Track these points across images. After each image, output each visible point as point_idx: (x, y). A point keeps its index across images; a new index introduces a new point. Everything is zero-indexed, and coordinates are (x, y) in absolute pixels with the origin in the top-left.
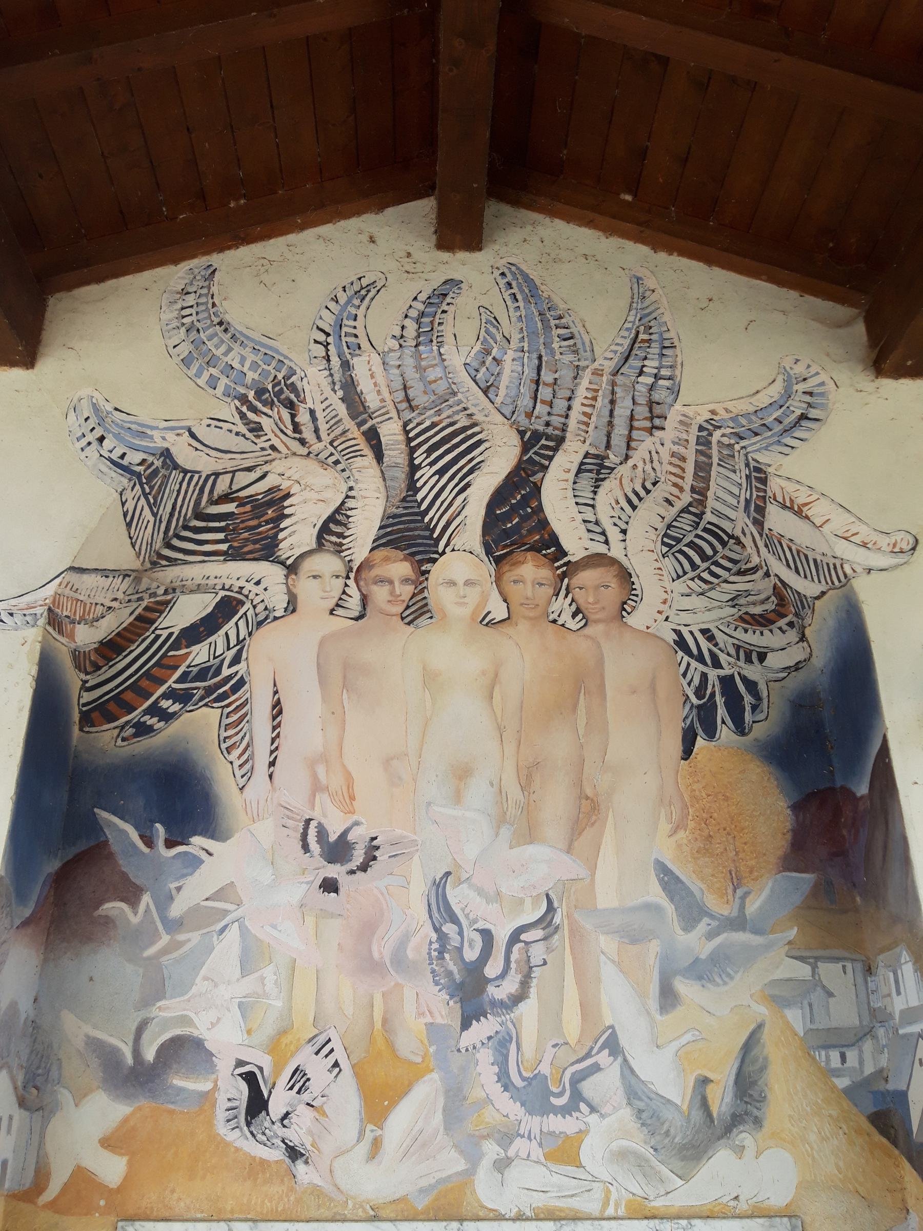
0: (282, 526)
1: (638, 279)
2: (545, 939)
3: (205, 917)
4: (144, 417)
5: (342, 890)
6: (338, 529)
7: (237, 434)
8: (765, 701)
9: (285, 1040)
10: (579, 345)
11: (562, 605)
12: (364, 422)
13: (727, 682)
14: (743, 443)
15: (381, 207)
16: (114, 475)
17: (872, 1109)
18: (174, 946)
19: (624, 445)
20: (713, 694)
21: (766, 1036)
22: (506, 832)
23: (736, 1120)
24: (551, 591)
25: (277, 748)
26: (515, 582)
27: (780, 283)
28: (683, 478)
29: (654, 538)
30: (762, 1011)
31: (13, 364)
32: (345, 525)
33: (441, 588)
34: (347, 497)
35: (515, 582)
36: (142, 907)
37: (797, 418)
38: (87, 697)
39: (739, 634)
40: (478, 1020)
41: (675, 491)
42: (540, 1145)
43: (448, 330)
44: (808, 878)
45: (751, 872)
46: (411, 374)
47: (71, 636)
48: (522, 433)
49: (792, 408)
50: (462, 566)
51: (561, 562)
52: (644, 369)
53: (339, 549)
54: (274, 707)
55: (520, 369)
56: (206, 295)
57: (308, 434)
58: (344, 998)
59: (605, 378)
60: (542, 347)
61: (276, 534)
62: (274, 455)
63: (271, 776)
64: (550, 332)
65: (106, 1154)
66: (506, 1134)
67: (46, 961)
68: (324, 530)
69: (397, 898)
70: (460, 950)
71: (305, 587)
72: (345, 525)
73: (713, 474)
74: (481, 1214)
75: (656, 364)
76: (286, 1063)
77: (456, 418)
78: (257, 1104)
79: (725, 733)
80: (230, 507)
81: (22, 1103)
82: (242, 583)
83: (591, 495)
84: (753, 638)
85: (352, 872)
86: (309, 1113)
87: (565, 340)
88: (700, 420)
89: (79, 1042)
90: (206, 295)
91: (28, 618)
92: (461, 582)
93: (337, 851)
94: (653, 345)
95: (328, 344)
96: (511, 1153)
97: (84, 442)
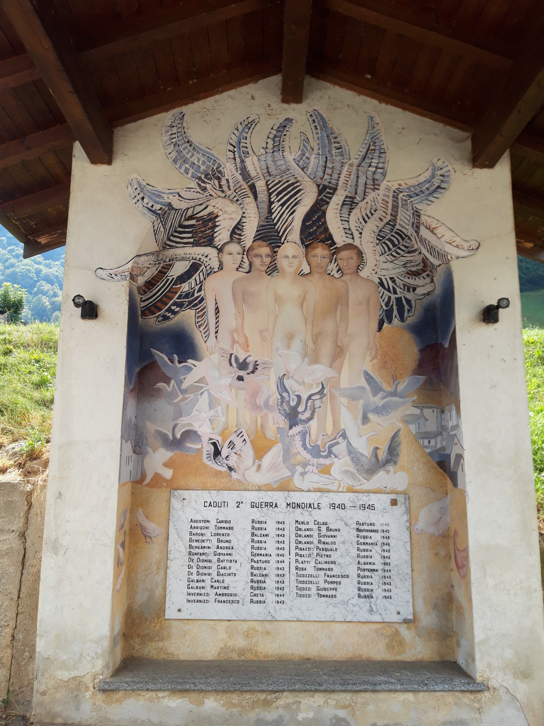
0: (215, 231)
1: (372, 118)
2: (320, 399)
3: (196, 389)
4: (159, 188)
5: (245, 380)
6: (239, 232)
7: (197, 192)
8: (414, 308)
9: (226, 432)
10: (344, 152)
11: (333, 267)
12: (249, 181)
13: (399, 300)
14: (412, 199)
15: (256, 81)
16: (149, 215)
17: (438, 460)
18: (185, 399)
19: (363, 194)
20: (392, 305)
21: (401, 434)
22: (307, 360)
23: (387, 462)
24: (329, 261)
25: (218, 326)
26: (314, 256)
27: (435, 120)
28: (387, 210)
29: (373, 236)
30: (400, 425)
31: (103, 163)
32: (242, 230)
33: (282, 259)
34: (242, 217)
35: (314, 256)
36: (171, 385)
37: (434, 188)
38: (143, 304)
39: (406, 280)
40: (295, 426)
41: (384, 214)
42: (317, 468)
43: (286, 144)
44: (423, 378)
45: (401, 375)
46: (270, 163)
47: (137, 282)
48: (318, 186)
49: (434, 183)
50: (291, 249)
51: (333, 247)
52: (372, 164)
53: (239, 241)
54: (216, 310)
55: (318, 162)
56: (181, 127)
57: (225, 188)
58: (247, 417)
59: (354, 168)
60: (327, 153)
61: (213, 234)
62: (211, 198)
63: (216, 337)
64: (331, 145)
65: (165, 469)
66: (305, 464)
67: (138, 403)
68: (233, 232)
69: (266, 384)
70: (289, 402)
71: (226, 259)
72: (242, 230)
73: (399, 210)
74: (296, 489)
75: (376, 161)
76: (227, 439)
77: (289, 179)
78: (217, 453)
79: (396, 321)
80: (193, 222)
81: (134, 452)
82: (200, 256)
83: (347, 216)
84: (411, 281)
85: (249, 374)
86: (235, 456)
87: (338, 149)
88: (394, 188)
89: (153, 432)
90: (181, 127)
91: (123, 277)
92: (291, 256)
93: (243, 366)
94: (376, 152)
95: (235, 151)
96: (306, 470)
97: (136, 200)
